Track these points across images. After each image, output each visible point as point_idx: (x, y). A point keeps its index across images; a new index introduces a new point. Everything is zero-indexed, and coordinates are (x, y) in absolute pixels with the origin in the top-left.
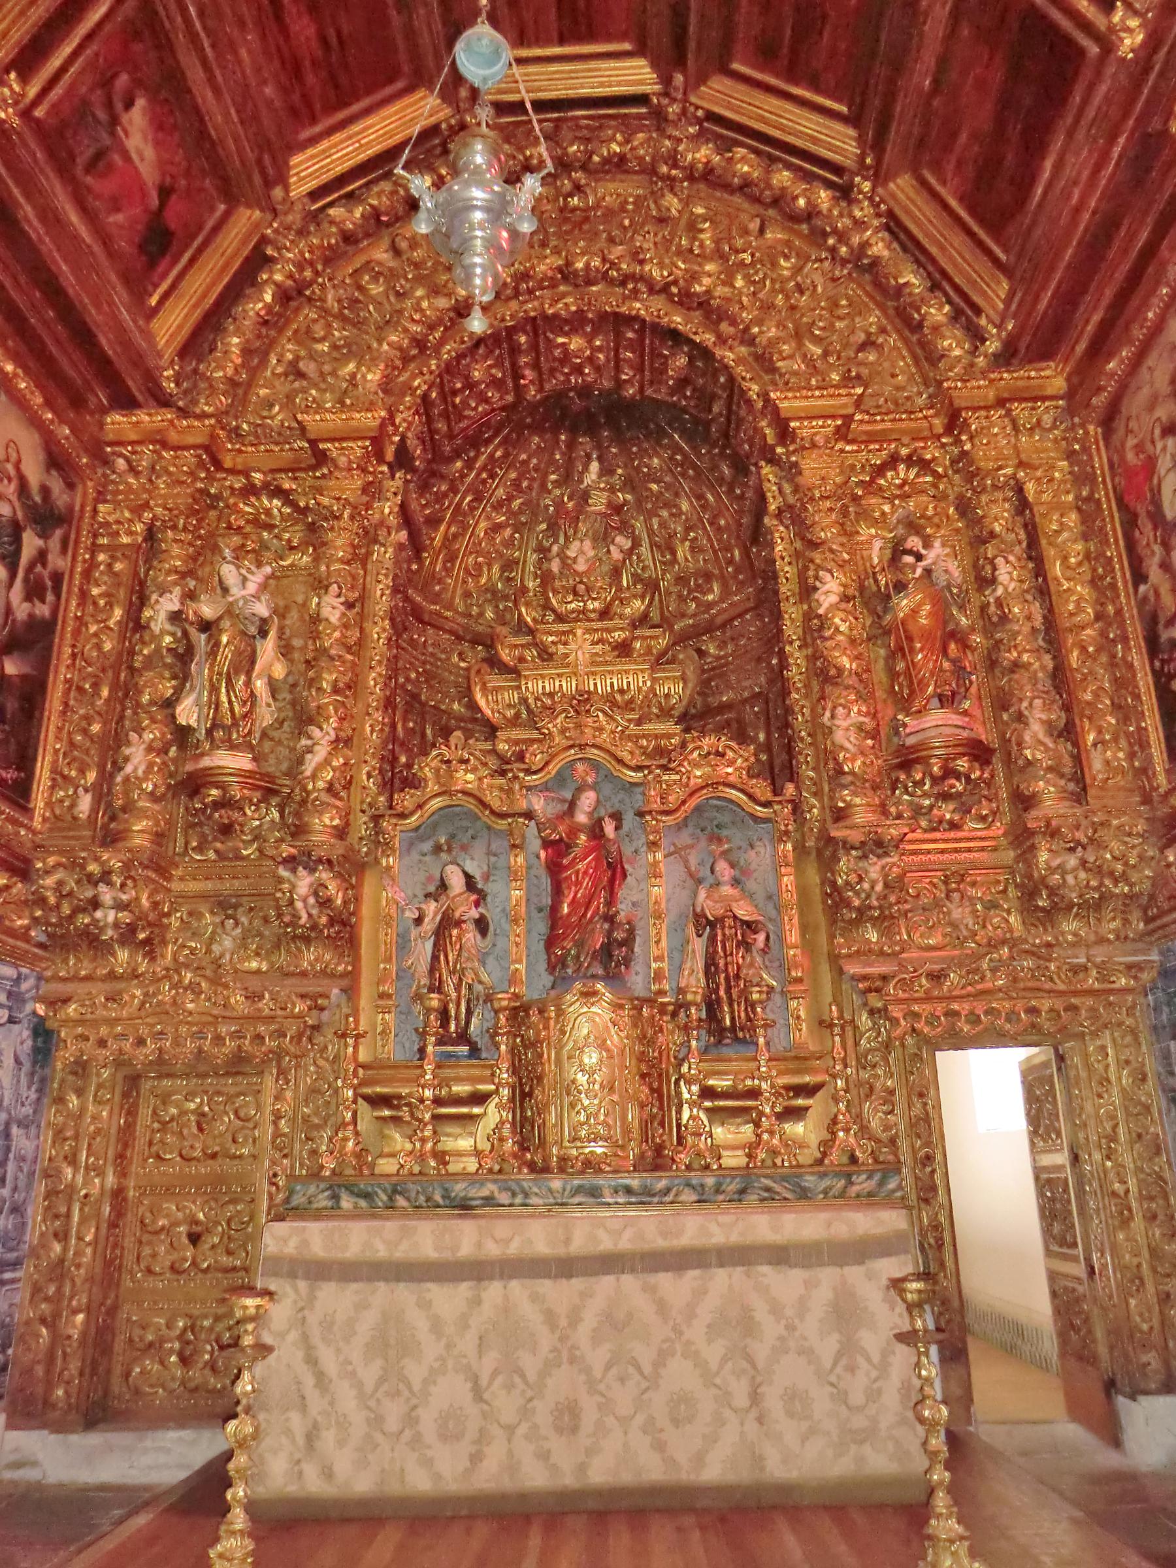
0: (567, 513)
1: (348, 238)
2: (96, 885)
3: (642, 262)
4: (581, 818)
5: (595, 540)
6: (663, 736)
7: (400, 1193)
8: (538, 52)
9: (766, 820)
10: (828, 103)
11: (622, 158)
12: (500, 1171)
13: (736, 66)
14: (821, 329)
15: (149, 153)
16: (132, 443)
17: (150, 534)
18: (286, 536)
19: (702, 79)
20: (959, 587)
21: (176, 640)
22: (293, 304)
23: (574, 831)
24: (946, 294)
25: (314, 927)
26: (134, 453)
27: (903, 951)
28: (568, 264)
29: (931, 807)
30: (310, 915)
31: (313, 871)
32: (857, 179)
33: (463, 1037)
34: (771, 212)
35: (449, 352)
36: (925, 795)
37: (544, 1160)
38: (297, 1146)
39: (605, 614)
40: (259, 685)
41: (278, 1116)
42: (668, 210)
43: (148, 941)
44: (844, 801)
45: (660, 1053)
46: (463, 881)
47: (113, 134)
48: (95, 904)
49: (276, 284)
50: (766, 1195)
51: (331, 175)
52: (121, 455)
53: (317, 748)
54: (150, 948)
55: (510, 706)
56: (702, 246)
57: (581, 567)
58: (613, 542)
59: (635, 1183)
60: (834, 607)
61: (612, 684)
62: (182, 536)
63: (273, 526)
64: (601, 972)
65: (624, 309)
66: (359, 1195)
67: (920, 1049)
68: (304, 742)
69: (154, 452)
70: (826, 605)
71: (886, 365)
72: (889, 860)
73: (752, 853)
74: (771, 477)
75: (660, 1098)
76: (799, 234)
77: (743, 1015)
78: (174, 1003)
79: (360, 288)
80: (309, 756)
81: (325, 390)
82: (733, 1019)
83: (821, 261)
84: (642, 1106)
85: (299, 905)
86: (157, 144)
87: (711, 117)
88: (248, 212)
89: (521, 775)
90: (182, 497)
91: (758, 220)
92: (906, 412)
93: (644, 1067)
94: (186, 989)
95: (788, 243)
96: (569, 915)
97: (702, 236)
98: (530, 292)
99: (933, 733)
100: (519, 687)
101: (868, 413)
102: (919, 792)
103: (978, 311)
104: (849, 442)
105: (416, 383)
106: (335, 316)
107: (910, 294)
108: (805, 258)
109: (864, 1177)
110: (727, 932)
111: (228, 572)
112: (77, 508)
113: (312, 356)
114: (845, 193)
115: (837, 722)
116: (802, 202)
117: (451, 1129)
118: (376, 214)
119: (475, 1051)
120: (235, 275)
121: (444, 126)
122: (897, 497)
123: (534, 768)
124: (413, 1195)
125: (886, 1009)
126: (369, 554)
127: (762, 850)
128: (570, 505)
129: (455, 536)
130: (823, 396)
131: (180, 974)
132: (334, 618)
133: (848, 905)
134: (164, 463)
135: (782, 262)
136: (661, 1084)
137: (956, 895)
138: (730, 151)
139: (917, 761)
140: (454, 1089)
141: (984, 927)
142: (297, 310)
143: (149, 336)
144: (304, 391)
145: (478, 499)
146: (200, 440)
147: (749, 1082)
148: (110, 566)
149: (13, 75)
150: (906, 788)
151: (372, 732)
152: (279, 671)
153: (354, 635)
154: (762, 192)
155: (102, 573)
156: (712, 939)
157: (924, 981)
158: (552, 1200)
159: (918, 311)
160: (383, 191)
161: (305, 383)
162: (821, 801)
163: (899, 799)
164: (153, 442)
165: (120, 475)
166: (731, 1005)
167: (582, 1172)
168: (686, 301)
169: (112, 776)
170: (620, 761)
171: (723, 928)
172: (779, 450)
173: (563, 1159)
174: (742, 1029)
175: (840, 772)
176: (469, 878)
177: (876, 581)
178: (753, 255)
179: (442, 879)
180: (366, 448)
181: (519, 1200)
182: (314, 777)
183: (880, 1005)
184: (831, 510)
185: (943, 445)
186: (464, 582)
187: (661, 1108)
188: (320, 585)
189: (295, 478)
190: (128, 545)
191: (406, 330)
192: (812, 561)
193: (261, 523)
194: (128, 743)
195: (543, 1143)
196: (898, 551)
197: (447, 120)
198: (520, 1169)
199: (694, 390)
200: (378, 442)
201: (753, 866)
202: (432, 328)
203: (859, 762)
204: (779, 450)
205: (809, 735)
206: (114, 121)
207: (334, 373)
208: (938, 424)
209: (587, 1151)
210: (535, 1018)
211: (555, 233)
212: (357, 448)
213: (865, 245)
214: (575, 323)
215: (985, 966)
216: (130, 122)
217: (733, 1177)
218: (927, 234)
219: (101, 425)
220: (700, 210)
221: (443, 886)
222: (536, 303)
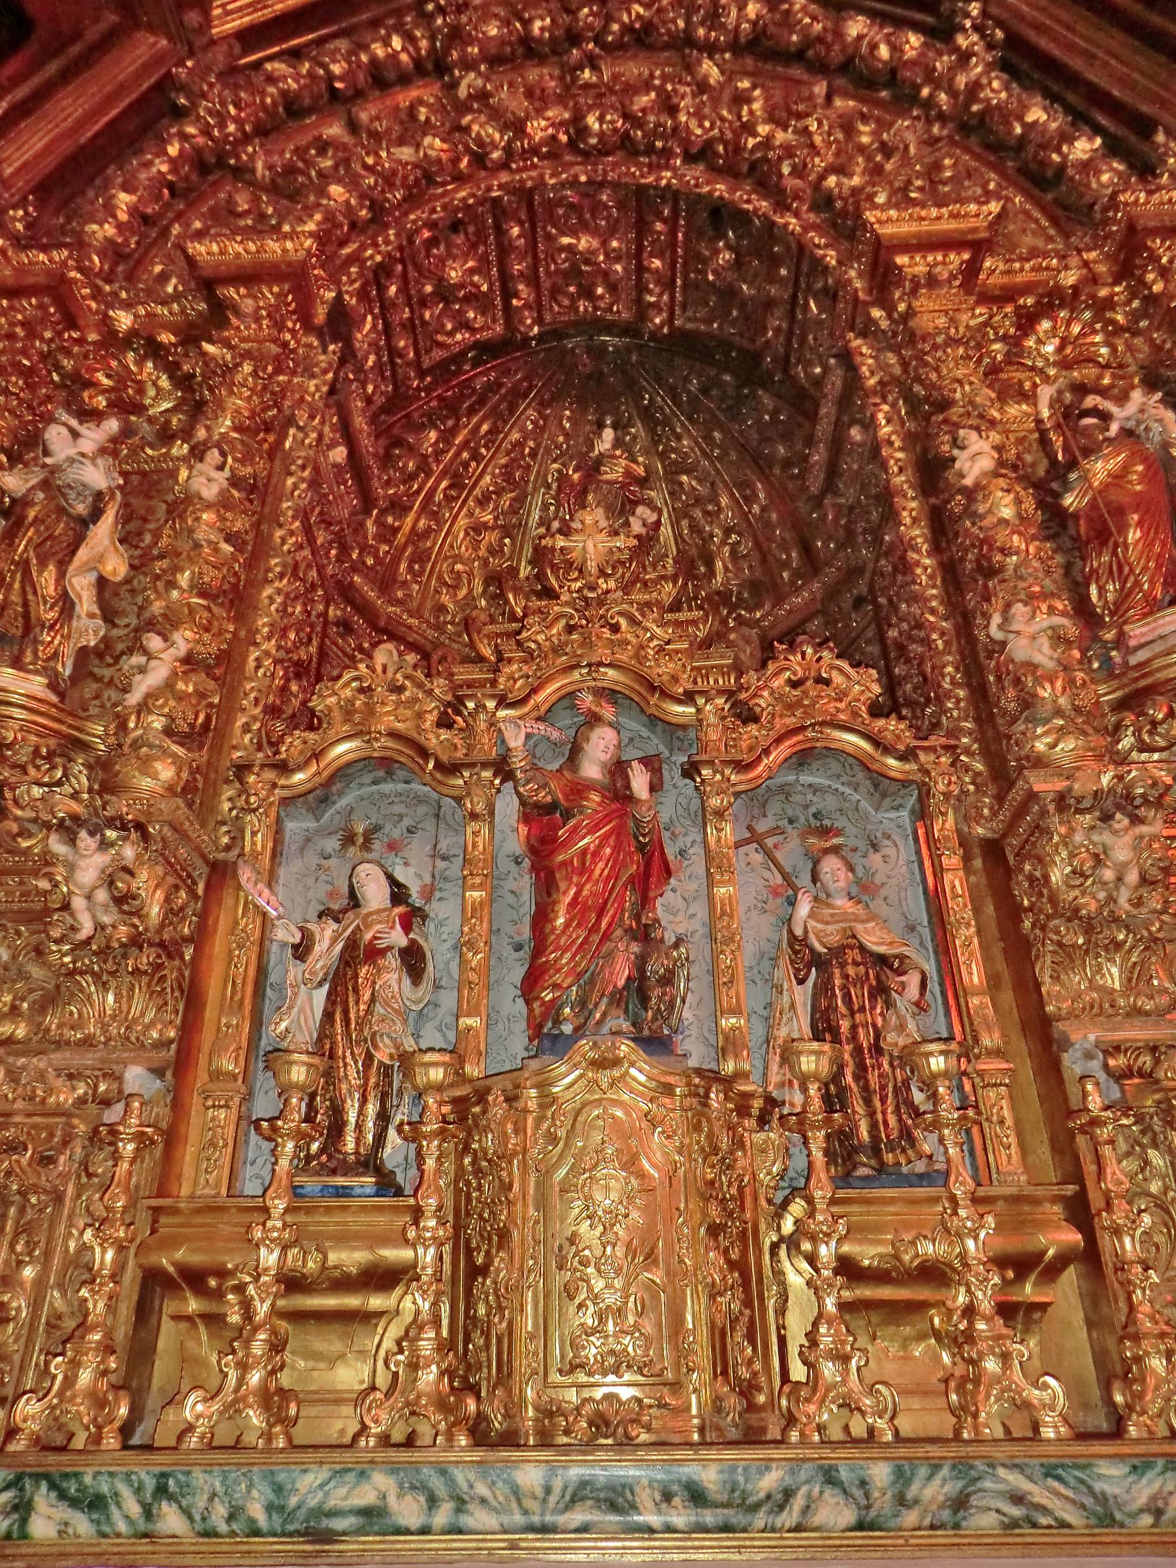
0: (572, 486)
4: (592, 769)
7: (171, 1498)
9: (905, 783)
11: (649, 26)
12: (410, 1442)
22: (211, 178)
23: (579, 790)
30: (99, 927)
33: (370, 1163)
34: (840, 82)
37: (507, 1416)
40: (82, 586)
45: (741, 1189)
46: (387, 892)
50: (1016, 1512)
64: (626, 1026)
66: (74, 1503)
73: (876, 859)
74: (864, 350)
75: (746, 1284)
77: (892, 1121)
80: (138, 678)
82: (874, 1127)
84: (714, 1294)
85: (78, 903)
88: (152, 39)
93: (714, 1212)
110: (851, 970)
117: (326, 1341)
124: (201, 1502)
127: (891, 852)
128: (576, 476)
129: (428, 531)
136: (744, 1252)
140: (333, 1258)
142: (216, 185)
145: (457, 484)
147: (927, 1249)
152: (116, 566)
156: (824, 989)
158: (519, 1519)
166: (868, 1102)
167: (589, 1445)
171: (842, 966)
173: (549, 1413)
176: (398, 893)
181: (442, 1517)
182: (143, 708)
186: (437, 592)
187: (747, 1303)
195: (504, 1377)
198: (450, 1438)
201: (879, 879)
209: (598, 1394)
210: (498, 1110)
217: (936, 1468)
221: (354, 900)
222: (534, 174)
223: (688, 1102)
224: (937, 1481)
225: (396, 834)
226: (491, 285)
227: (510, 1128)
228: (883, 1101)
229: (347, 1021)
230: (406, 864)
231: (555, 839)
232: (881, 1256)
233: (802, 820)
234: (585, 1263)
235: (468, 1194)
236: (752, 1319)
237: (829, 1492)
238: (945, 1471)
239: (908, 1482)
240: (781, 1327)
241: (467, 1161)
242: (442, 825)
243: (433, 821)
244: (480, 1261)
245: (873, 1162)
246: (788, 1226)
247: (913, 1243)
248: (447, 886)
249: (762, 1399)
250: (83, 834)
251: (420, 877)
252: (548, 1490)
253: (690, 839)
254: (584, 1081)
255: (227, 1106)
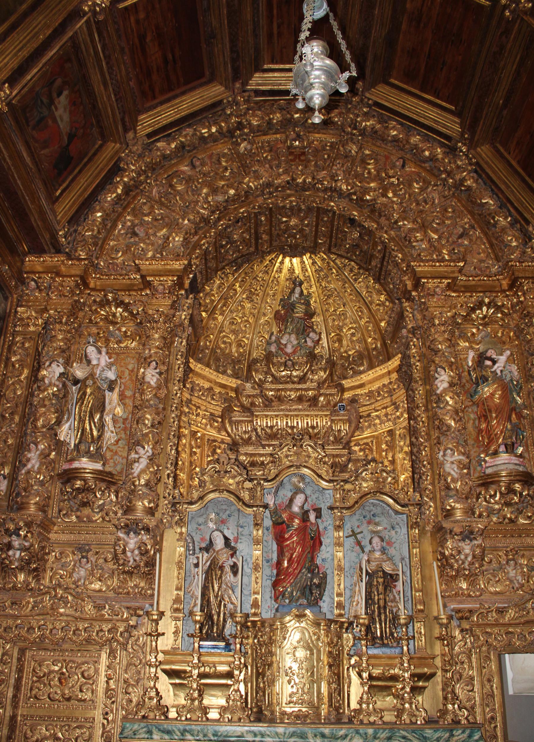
1: (164, 157)
2: (10, 536)
3: (336, 181)
4: (296, 509)
5: (297, 334)
6: (337, 456)
8: (282, 66)
10: (444, 104)
13: (392, 81)
14: (437, 224)
15: (66, 117)
16: (39, 273)
17: (46, 323)
18: (124, 329)
19: (373, 85)
20: (517, 382)
21: (58, 390)
23: (292, 517)
24: (509, 211)
25: (137, 567)
26: (39, 278)
27: (481, 595)
28: (293, 179)
29: (500, 510)
30: (135, 560)
31: (137, 533)
32: (460, 144)
35: (222, 225)
36: (496, 503)
38: (120, 696)
39: (302, 379)
41: (109, 678)
42: (350, 151)
43: (35, 570)
44: (451, 506)
45: (339, 652)
47: (49, 109)
48: (9, 546)
49: (125, 183)
51: (160, 125)
52: (33, 280)
53: (141, 460)
54: (37, 574)
55: (245, 432)
56: (369, 173)
57: (289, 350)
58: (308, 336)
59: (327, 731)
60: (445, 390)
61: (307, 423)
62: (65, 328)
63: (117, 323)
65: (324, 206)
67: (489, 653)
68: (133, 456)
69: (51, 278)
70: (441, 389)
71: (475, 246)
72: (476, 542)
73: (393, 532)
74: (408, 309)
76: (425, 169)
78: (52, 609)
79: (171, 186)
80: (136, 464)
81: (148, 244)
83: (437, 185)
85: (129, 554)
86: (71, 112)
87: (377, 104)
89: (262, 482)
90: (66, 304)
91: (402, 160)
92: (486, 276)
94: (59, 600)
95: (418, 174)
96: (288, 567)
97: (369, 167)
98: (270, 193)
99: (502, 467)
100: (252, 421)
101: (465, 276)
102: (492, 501)
103: (528, 222)
104: (454, 291)
105: (202, 242)
106: (156, 202)
107: (489, 209)
108: (427, 184)
109: (460, 732)
111: (91, 350)
112: (8, 311)
113: (142, 223)
114: (452, 151)
115: (446, 458)
116: (427, 153)
118: (183, 146)
119: (228, 645)
120: (103, 178)
121: (225, 101)
122: (481, 324)
123: (270, 478)
125: (471, 630)
126: (172, 342)
127: (399, 530)
130: (440, 266)
131: (56, 591)
132: (153, 382)
133: (452, 567)
134: (56, 284)
135: (415, 184)
137: (512, 562)
138: (386, 122)
139: (492, 483)
141: (528, 582)
143: (54, 212)
144: (136, 244)
146: (78, 272)
148: (23, 344)
149: (7, 85)
150: (485, 498)
151: (171, 450)
153: (163, 393)
154: (404, 146)
155: (18, 348)
157: (494, 614)
159: (493, 218)
160: (188, 134)
161: (137, 239)
162: (435, 503)
163: (481, 504)
164: (51, 272)
165: (31, 291)
166: (381, 624)
168: (360, 203)
169: (19, 470)
170: (320, 476)
172: (414, 293)
174: (386, 638)
175: (448, 488)
177: (470, 374)
178: (398, 179)
179: (210, 539)
180: (173, 281)
183: (468, 627)
184: (444, 332)
185: (507, 296)
188: (146, 361)
189: (130, 295)
190: (33, 332)
191: (198, 212)
192: (434, 361)
193: (111, 320)
194: (29, 451)
196: (481, 357)
197: (227, 98)
199: (361, 251)
200: (181, 280)
201: (393, 540)
202: (213, 212)
203: (459, 483)
204: (414, 293)
205: (429, 464)
206: (52, 102)
207: (155, 235)
208: (505, 283)
211: (285, 161)
212: (170, 280)
213: (463, 180)
214: (294, 211)
215: (530, 606)
216: (59, 103)
217: (384, 729)
218: (499, 178)
219: (23, 262)
220: (367, 152)
223: (325, 627)
224: (384, 733)
225: (224, 517)
226: (250, 236)
227: (272, 634)
228: (385, 624)
229: (213, 591)
230: (228, 529)
231: (284, 537)
232: (379, 673)
233: (368, 517)
234: (294, 674)
235: (256, 651)
236: (340, 689)
237: (357, 735)
238: (387, 731)
239: (377, 733)
240: (348, 691)
241: (256, 641)
242: (241, 514)
243: (237, 512)
244: (261, 671)
245: (381, 642)
246: (353, 661)
247: (388, 670)
248: (243, 537)
249: (341, 711)
250: (132, 533)
251: (233, 533)
252: (285, 733)
253: (328, 523)
254: (294, 621)
255: (179, 620)
